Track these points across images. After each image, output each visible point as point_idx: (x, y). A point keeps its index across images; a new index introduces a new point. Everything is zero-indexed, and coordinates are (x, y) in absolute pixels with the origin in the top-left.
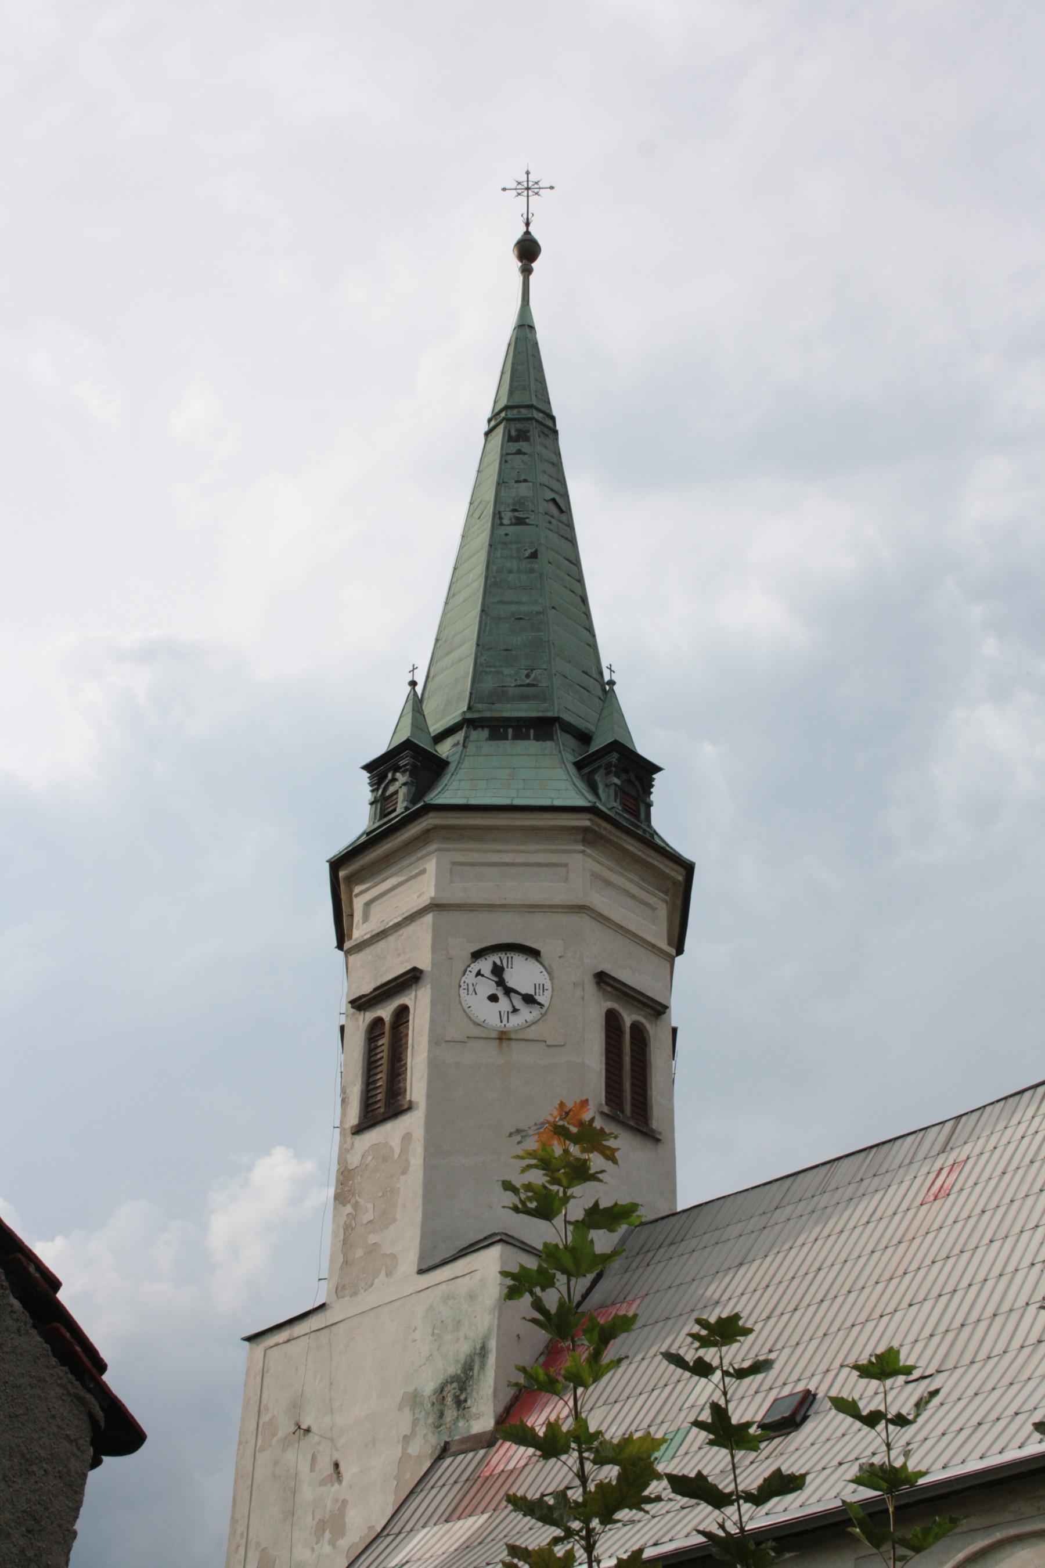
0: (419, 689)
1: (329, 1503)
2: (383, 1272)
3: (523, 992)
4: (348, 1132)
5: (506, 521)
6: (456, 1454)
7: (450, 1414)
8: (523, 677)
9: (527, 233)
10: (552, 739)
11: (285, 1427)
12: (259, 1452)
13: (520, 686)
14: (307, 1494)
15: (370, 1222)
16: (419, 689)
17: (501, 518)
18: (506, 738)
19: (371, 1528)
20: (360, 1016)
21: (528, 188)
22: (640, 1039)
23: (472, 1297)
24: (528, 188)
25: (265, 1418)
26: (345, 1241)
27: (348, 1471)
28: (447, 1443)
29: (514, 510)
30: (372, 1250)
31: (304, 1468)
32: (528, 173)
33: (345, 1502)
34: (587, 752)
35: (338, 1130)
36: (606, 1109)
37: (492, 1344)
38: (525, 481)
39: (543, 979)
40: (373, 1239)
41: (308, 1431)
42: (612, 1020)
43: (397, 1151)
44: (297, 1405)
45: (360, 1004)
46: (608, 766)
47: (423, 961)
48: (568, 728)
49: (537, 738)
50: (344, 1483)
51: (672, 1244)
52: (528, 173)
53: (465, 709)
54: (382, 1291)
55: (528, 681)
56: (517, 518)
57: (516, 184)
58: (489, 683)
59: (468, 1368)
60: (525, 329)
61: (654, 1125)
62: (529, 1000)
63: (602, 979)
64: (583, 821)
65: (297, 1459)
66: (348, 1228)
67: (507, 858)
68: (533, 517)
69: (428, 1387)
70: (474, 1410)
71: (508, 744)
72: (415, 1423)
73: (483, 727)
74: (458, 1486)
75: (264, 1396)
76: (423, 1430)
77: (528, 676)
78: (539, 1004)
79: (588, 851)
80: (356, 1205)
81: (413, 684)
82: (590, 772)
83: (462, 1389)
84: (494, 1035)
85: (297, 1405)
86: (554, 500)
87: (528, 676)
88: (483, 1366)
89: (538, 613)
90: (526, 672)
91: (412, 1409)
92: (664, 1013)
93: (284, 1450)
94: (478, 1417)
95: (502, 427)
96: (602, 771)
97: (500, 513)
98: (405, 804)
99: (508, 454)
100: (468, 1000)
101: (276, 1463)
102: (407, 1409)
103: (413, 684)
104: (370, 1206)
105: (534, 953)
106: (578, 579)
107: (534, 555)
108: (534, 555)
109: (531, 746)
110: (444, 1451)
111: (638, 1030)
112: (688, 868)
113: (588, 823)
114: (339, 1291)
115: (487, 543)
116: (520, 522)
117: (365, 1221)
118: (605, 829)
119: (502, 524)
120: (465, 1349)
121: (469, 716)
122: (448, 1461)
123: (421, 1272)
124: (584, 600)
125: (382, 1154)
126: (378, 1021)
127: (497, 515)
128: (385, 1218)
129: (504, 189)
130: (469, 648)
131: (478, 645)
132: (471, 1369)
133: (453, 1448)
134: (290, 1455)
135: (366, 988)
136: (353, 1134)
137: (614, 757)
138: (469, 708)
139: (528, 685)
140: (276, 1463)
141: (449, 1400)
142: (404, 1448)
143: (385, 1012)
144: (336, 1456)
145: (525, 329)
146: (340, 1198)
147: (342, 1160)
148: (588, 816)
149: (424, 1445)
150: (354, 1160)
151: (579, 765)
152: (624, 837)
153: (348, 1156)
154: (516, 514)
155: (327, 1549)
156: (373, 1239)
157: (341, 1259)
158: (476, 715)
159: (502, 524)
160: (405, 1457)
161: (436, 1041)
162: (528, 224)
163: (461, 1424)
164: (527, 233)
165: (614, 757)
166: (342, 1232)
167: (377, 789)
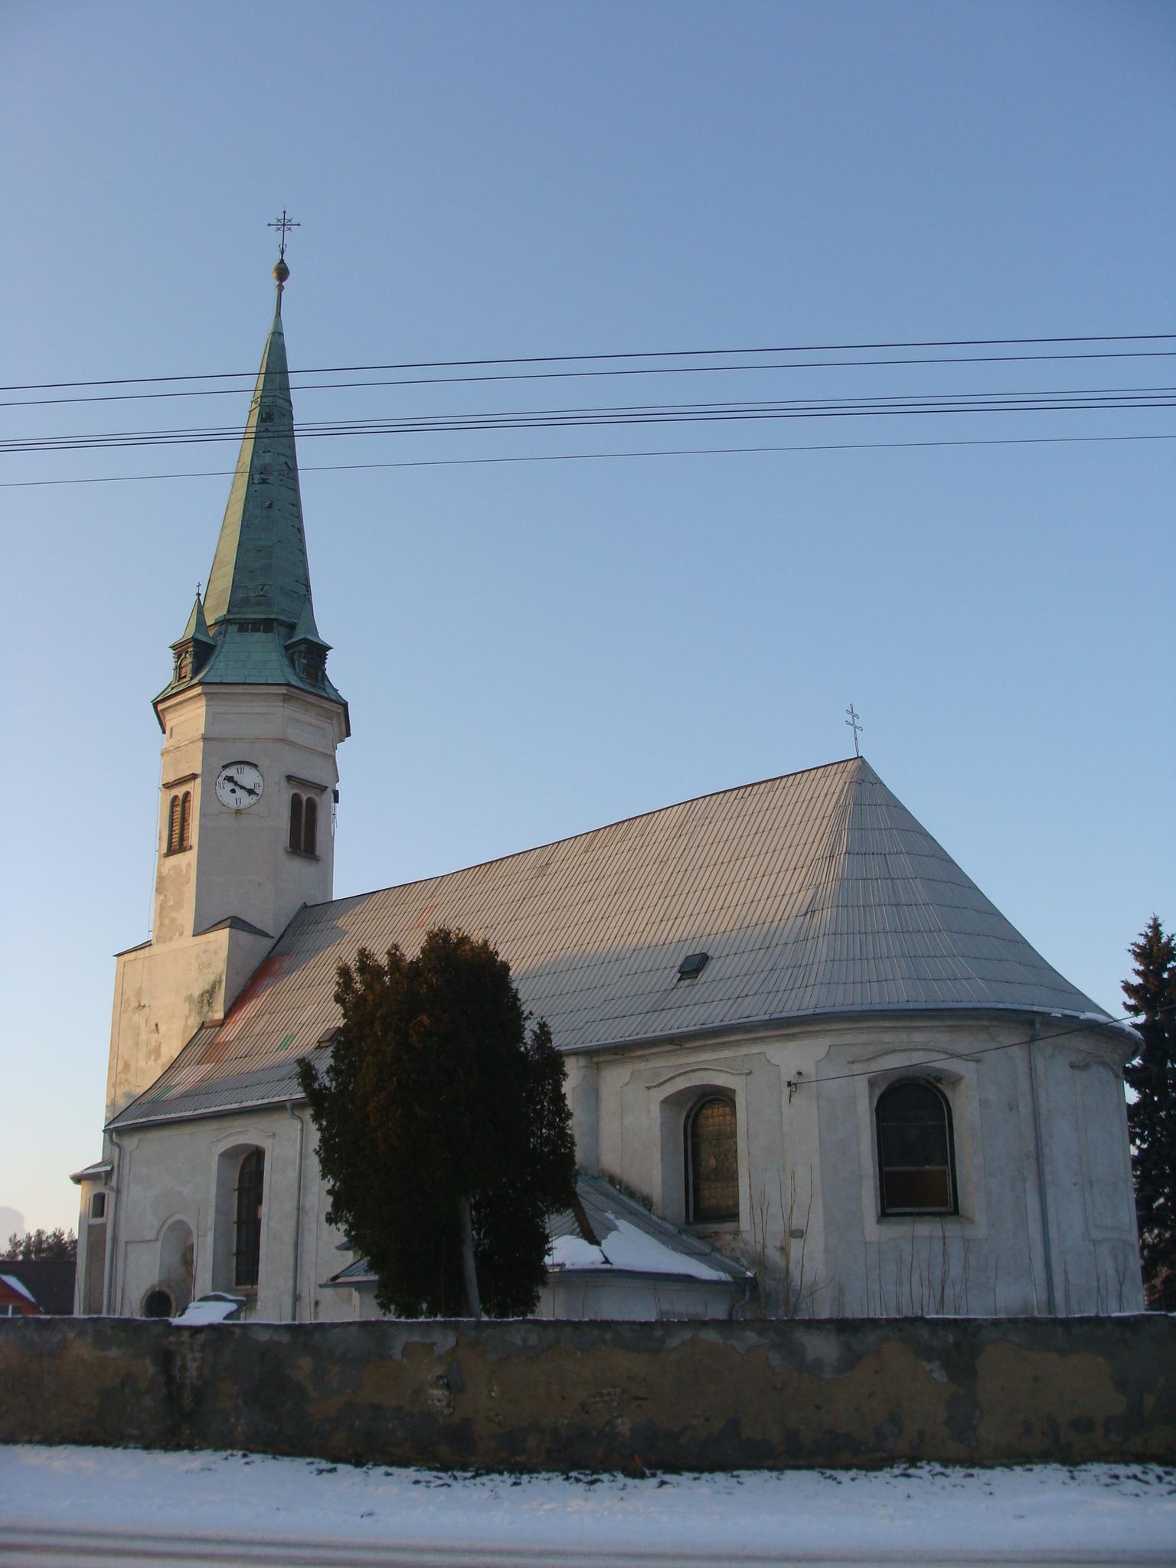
0: (202, 598)
1: (154, 1043)
2: (177, 934)
3: (248, 788)
4: (162, 856)
5: (256, 481)
6: (208, 1028)
7: (206, 1008)
8: (259, 590)
9: (282, 261)
10: (272, 632)
11: (134, 1004)
12: (123, 1012)
13: (258, 596)
14: (144, 1036)
15: (172, 906)
16: (202, 598)
17: (253, 479)
18: (247, 631)
19: (172, 1057)
20: (167, 791)
21: (284, 225)
22: (312, 805)
23: (216, 953)
24: (284, 225)
25: (125, 997)
26: (161, 913)
27: (162, 1028)
28: (203, 1022)
29: (261, 473)
30: (173, 920)
31: (142, 1023)
32: (284, 212)
33: (160, 1043)
34: (292, 637)
35: (157, 853)
36: (289, 850)
37: (224, 978)
38: (269, 451)
39: (259, 780)
40: (173, 915)
41: (144, 1006)
42: (296, 800)
43: (185, 871)
44: (139, 992)
45: (168, 786)
46: (301, 652)
47: (198, 771)
48: (281, 623)
49: (265, 631)
50: (160, 1034)
51: (315, 924)
52: (284, 212)
53: (226, 613)
54: (177, 943)
55: (262, 593)
56: (262, 479)
57: (276, 221)
58: (240, 595)
59: (213, 987)
60: (277, 334)
61: (317, 852)
62: (251, 792)
63: (290, 778)
64: (283, 690)
65: (138, 1018)
66: (162, 907)
67: (243, 710)
68: (271, 478)
69: (197, 993)
70: (215, 1008)
71: (248, 634)
72: (190, 1011)
73: (235, 623)
74: (205, 1046)
75: (124, 985)
76: (194, 1014)
77: (262, 590)
78: (257, 794)
79: (286, 705)
80: (165, 896)
81: (199, 595)
82: (293, 653)
83: (211, 997)
84: (233, 811)
85: (139, 992)
86: (280, 474)
87: (262, 590)
88: (219, 988)
89: (270, 546)
90: (261, 587)
91: (190, 1004)
92: (326, 790)
93: (134, 1014)
94: (217, 1012)
95: (258, 408)
96: (297, 653)
97: (253, 475)
98: (191, 675)
99: (260, 432)
100: (220, 792)
101: (130, 1020)
102: (187, 1003)
103: (199, 595)
104: (172, 898)
105: (255, 766)
106: (296, 515)
107: (270, 506)
108: (270, 506)
109: (260, 636)
110: (202, 1026)
111: (311, 802)
112: (345, 705)
113: (285, 692)
114: (160, 939)
115: (244, 497)
116: (264, 481)
117: (170, 905)
118: (295, 693)
119: (253, 483)
120: (212, 978)
121: (227, 617)
122: (204, 1031)
123: (194, 935)
124: (300, 530)
125: (176, 869)
126: (176, 797)
127: (251, 477)
128: (178, 906)
129: (269, 225)
130: (230, 569)
131: (235, 568)
132: (215, 988)
133: (206, 1025)
134: (136, 1017)
135: (171, 778)
136: (165, 857)
137: (303, 647)
138: (228, 612)
139: (262, 596)
140: (130, 1020)
141: (205, 1001)
142: (186, 1021)
143: (179, 791)
144: (157, 1021)
145: (277, 334)
146: (159, 890)
147: (159, 871)
148: (285, 687)
149: (194, 1022)
150: (165, 871)
151: (287, 648)
152: (306, 694)
153: (162, 870)
154: (263, 476)
155: (151, 1063)
156: (173, 915)
157: (158, 923)
158: (231, 617)
159: (253, 483)
160: (186, 1026)
161: (203, 815)
162: (282, 253)
163: (210, 1013)
164: (282, 261)
165: (303, 647)
166: (159, 909)
167: (178, 661)
